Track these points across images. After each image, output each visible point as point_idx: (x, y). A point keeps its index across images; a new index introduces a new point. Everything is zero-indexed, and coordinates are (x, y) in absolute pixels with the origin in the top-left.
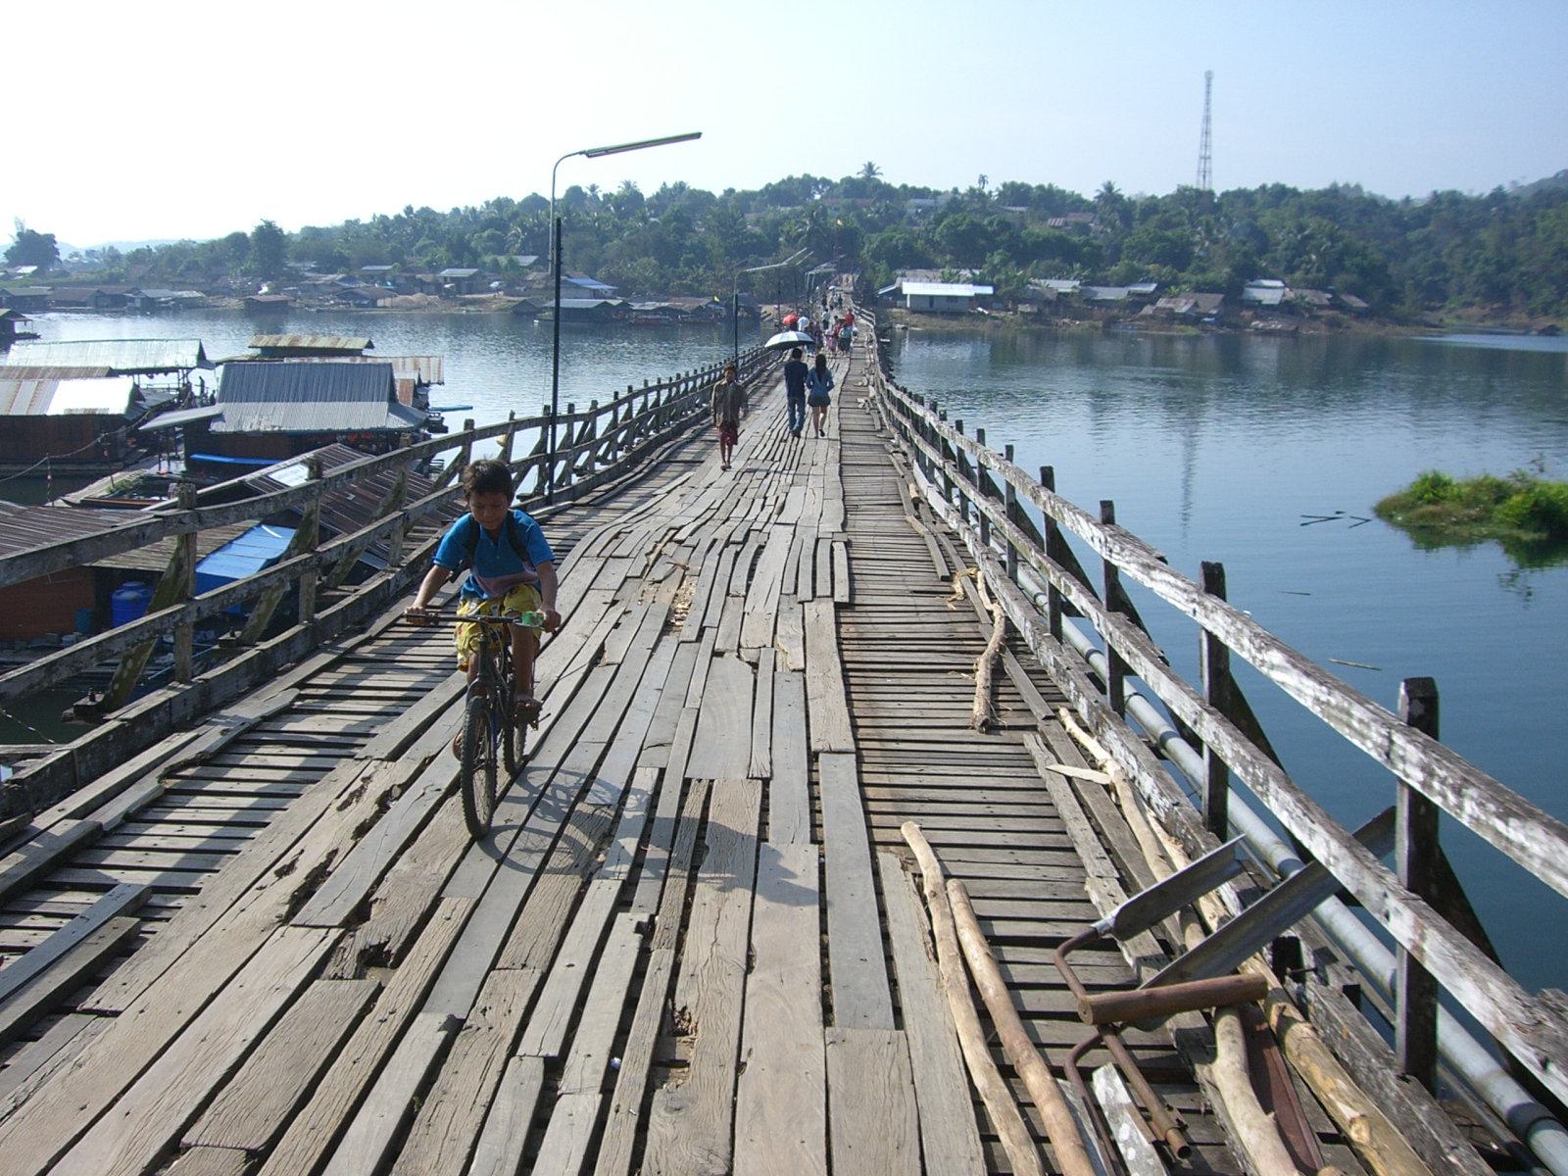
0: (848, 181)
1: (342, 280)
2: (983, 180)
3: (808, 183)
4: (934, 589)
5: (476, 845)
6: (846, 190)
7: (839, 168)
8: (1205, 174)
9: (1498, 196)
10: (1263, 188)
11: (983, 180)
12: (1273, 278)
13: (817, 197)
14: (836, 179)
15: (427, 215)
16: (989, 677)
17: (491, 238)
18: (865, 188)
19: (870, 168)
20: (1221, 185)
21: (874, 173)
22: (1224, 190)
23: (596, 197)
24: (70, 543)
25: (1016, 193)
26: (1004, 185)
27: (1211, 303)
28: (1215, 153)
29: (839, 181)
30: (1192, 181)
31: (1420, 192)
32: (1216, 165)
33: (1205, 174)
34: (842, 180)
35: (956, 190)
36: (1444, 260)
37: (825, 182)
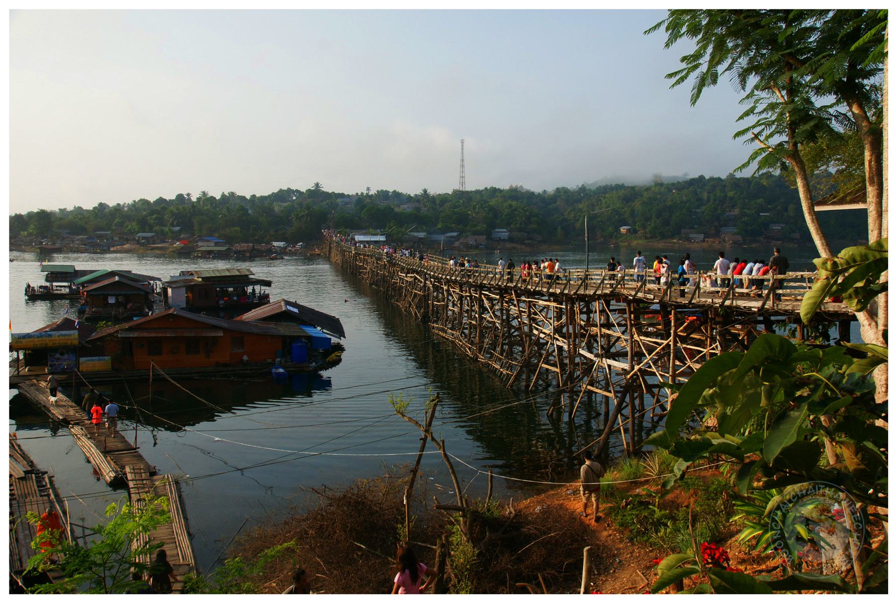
0: (309, 191)
1: (87, 238)
2: (368, 189)
3: (290, 191)
4: (306, 416)
5: (173, 589)
6: (308, 195)
7: (304, 185)
8: (462, 184)
9: (583, 189)
10: (486, 189)
11: (368, 189)
12: (502, 228)
13: (294, 198)
14: (304, 190)
15: (144, 202)
16: (868, 317)
17: (156, 219)
18: (316, 193)
19: (317, 185)
20: (470, 187)
21: (319, 187)
22: (749, 117)
23: (189, 199)
24: (101, 337)
25: (383, 195)
26: (378, 191)
27: (482, 239)
28: (467, 174)
29: (305, 191)
30: (457, 187)
31: (551, 189)
32: (467, 180)
33: (462, 184)
34: (307, 190)
35: (357, 194)
36: (566, 217)
37: (297, 191)
